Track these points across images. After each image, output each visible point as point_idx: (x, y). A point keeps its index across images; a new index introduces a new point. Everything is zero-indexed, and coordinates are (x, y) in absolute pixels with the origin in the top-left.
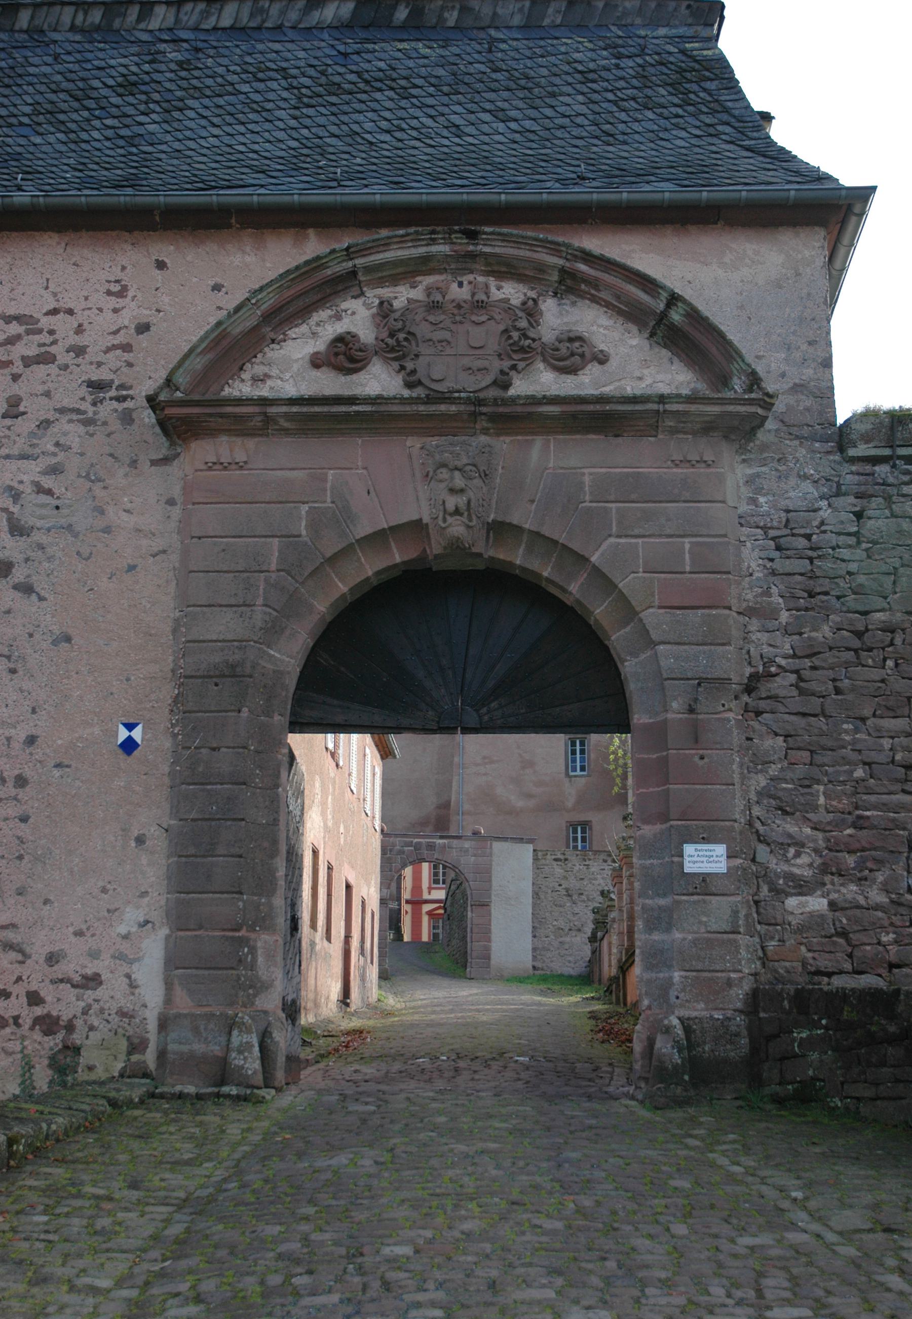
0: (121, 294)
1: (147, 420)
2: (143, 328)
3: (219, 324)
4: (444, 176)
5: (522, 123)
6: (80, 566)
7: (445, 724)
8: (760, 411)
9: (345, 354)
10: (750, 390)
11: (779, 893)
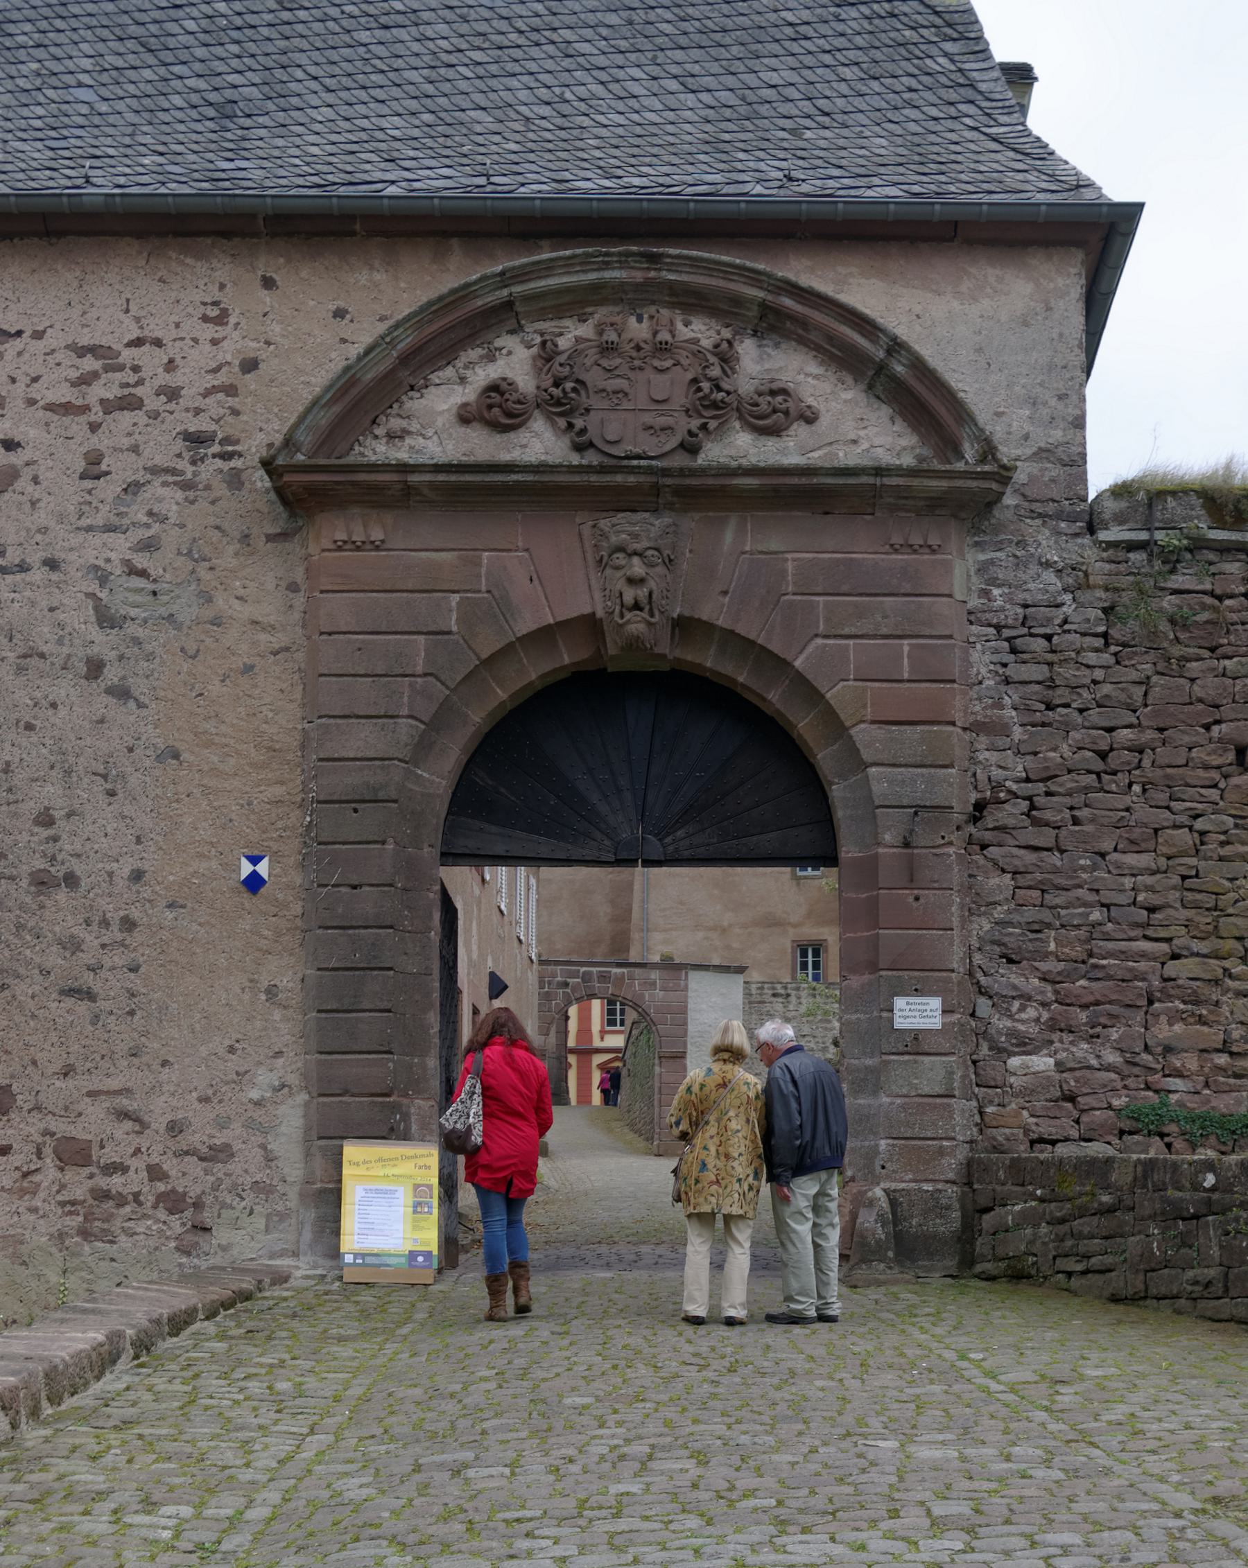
0: (221, 320)
1: (259, 484)
2: (250, 365)
3: (347, 369)
4: (619, 172)
5: (717, 94)
6: (185, 666)
7: (624, 855)
8: (994, 486)
9: (500, 406)
10: (983, 460)
11: (1001, 1052)
